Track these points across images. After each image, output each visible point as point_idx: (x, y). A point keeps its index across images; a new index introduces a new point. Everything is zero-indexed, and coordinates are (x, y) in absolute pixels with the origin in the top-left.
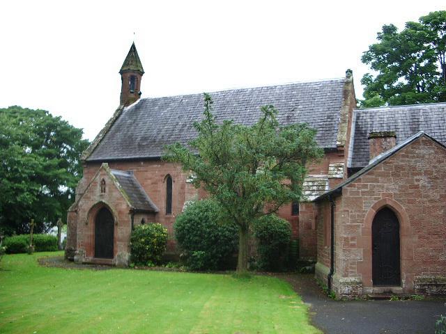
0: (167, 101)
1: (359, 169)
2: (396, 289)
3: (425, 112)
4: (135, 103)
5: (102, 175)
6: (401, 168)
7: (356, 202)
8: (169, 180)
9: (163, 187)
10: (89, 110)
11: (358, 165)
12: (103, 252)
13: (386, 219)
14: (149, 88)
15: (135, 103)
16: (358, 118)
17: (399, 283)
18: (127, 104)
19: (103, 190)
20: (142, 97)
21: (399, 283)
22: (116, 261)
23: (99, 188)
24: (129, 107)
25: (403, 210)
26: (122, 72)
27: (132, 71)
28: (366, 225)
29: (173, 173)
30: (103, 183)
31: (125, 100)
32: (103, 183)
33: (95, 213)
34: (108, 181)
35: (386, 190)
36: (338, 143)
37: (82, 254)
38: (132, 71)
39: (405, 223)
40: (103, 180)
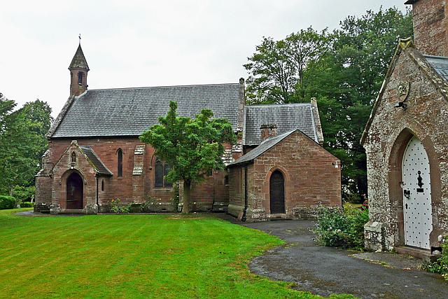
0: (110, 93)
1: (254, 147)
2: (282, 215)
3: (291, 109)
4: (83, 94)
5: (72, 149)
6: (286, 148)
7: (262, 168)
8: (120, 152)
9: (115, 158)
10: (57, 97)
11: (251, 143)
12: (75, 202)
13: (277, 175)
14: (94, 81)
15: (83, 94)
16: (247, 111)
17: (284, 212)
18: (77, 94)
19: (74, 160)
20: (88, 88)
21: (284, 212)
22: (86, 209)
23: (70, 159)
24: (79, 97)
25: (285, 171)
26: (71, 68)
27: (79, 67)
28: (266, 180)
29: (123, 148)
30: (74, 154)
31: (74, 91)
32: (74, 154)
33: (67, 177)
34: (78, 153)
35: (277, 161)
36: (238, 129)
37: (56, 206)
38: (79, 67)
39: (287, 179)
40: (74, 152)
